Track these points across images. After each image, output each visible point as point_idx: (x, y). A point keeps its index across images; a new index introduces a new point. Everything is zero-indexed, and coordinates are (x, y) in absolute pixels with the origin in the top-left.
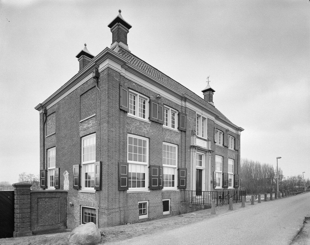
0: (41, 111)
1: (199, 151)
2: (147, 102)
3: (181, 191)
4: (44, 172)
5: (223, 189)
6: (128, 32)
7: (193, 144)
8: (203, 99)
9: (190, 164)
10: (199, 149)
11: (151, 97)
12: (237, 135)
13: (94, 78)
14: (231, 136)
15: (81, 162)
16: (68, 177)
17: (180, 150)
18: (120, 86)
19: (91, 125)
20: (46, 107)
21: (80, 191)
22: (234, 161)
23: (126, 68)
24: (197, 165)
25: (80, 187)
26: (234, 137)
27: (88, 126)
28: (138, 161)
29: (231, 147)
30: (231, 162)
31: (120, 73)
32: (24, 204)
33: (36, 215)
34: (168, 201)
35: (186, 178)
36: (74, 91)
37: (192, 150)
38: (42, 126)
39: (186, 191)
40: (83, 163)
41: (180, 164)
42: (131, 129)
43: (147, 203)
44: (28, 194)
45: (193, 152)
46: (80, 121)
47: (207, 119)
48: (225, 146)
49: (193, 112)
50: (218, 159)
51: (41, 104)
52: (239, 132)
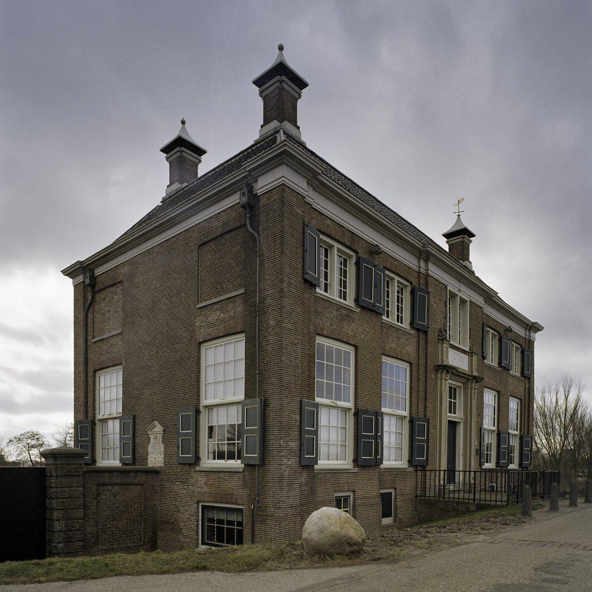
0: (80, 278)
1: (455, 378)
2: (350, 264)
4: (89, 425)
6: (299, 98)
7: (443, 360)
9: (435, 407)
12: (527, 341)
13: (244, 207)
14: (515, 344)
15: (198, 400)
16: (161, 435)
17: (414, 374)
18: (306, 227)
20: (92, 271)
21: (197, 468)
22: (521, 404)
23: (315, 186)
28: (326, 398)
29: (516, 371)
30: (513, 405)
31: (305, 197)
32: (69, 497)
33: (93, 524)
34: (391, 493)
35: (427, 441)
36: (180, 233)
38: (81, 316)
40: (204, 402)
42: (323, 325)
43: (350, 496)
44: (79, 476)
45: (441, 380)
46: (198, 306)
48: (503, 367)
49: (442, 285)
50: (489, 398)
52: (532, 334)
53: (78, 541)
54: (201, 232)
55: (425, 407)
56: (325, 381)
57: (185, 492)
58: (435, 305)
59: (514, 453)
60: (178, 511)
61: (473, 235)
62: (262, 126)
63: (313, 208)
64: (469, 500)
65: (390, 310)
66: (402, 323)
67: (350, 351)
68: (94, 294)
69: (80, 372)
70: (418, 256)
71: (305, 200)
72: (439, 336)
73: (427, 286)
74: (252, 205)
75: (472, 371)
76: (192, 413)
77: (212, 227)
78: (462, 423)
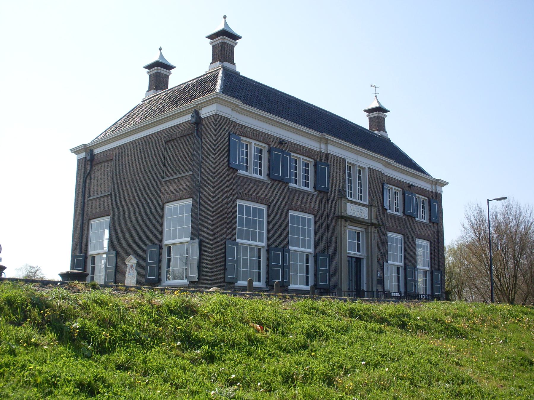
0: (83, 155)
1: (352, 224)
7: (342, 212)
11: (271, 143)
13: (193, 124)
15: (161, 240)
18: (230, 136)
19: (184, 186)
38: (81, 181)
46: (164, 180)
51: (85, 145)
58: (335, 174)
61: (387, 111)
62: (211, 64)
65: (297, 178)
66: (425, 219)
68: (92, 166)
69: (78, 221)
72: (338, 195)
74: (198, 121)
75: (371, 220)
76: (156, 249)
77: (174, 132)
78: (365, 259)
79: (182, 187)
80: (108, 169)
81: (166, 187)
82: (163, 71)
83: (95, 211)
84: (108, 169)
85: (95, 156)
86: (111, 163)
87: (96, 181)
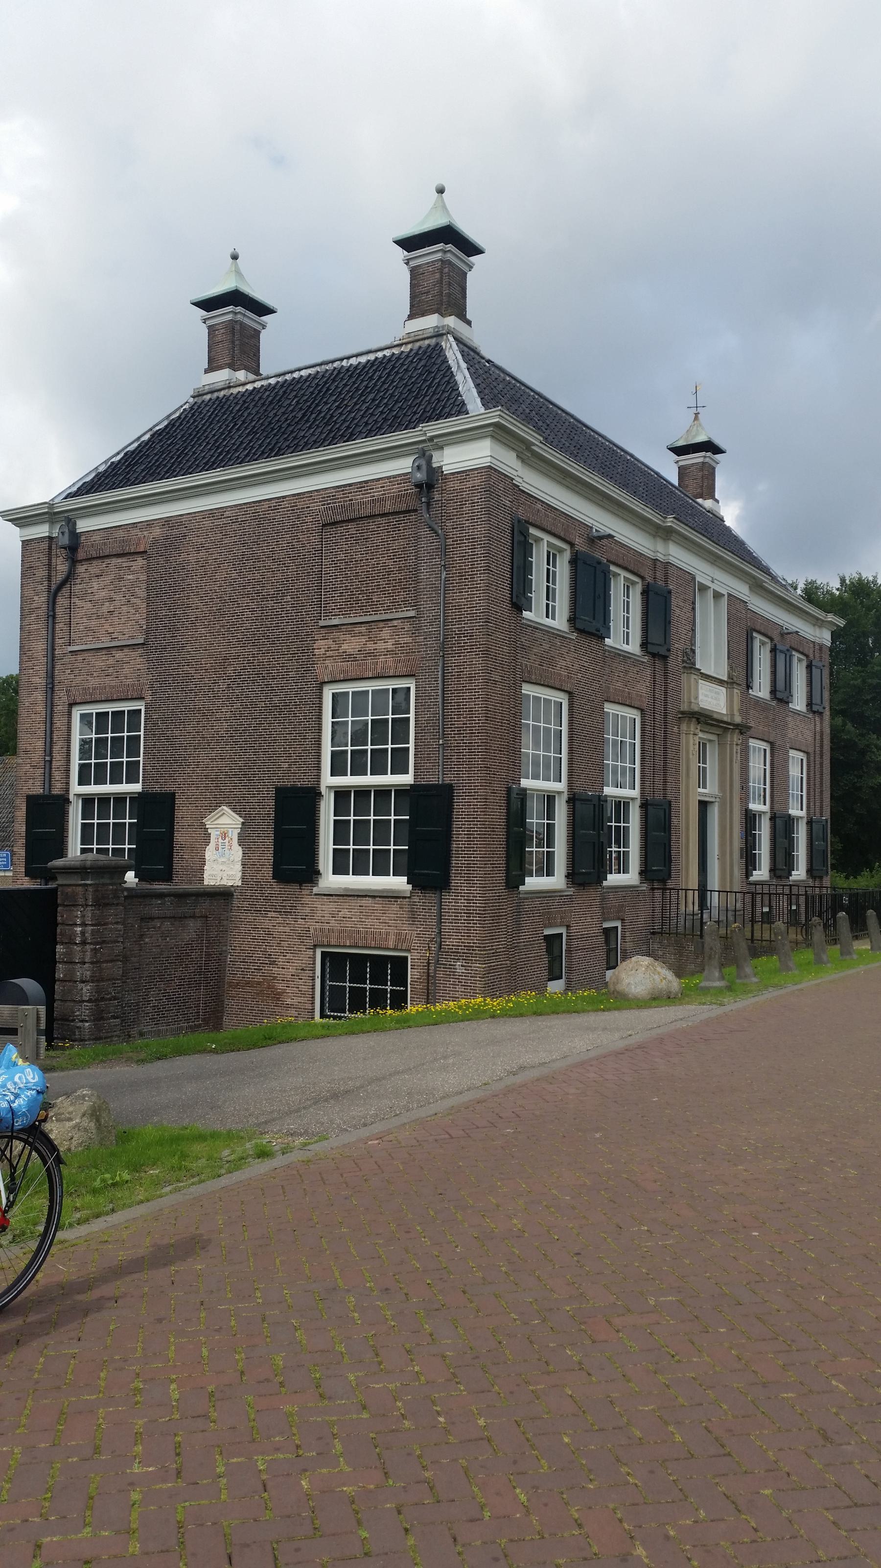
1: (707, 728)
3: (653, 889)
5: (774, 882)
8: (676, 483)
9: (677, 782)
10: (704, 719)
11: (577, 541)
12: (817, 647)
13: (419, 486)
19: (389, 645)
24: (699, 787)
25: (311, 875)
26: (807, 656)
27: (371, 646)
37: (684, 727)
39: (670, 889)
41: (647, 784)
47: (726, 596)
49: (687, 576)
53: (114, 1017)
54: (328, 504)
55: (665, 782)
56: (531, 751)
57: (287, 929)
59: (760, 830)
60: (273, 963)
63: (520, 489)
64: (762, 941)
67: (561, 700)
68: (74, 562)
70: (654, 533)
71: (514, 482)
72: (683, 661)
73: (666, 581)
75: (732, 715)
77: (352, 500)
79: (381, 646)
80: (129, 577)
81: (330, 642)
82: (249, 318)
83: (93, 682)
84: (129, 577)
85: (83, 538)
86: (140, 562)
87: (89, 605)
